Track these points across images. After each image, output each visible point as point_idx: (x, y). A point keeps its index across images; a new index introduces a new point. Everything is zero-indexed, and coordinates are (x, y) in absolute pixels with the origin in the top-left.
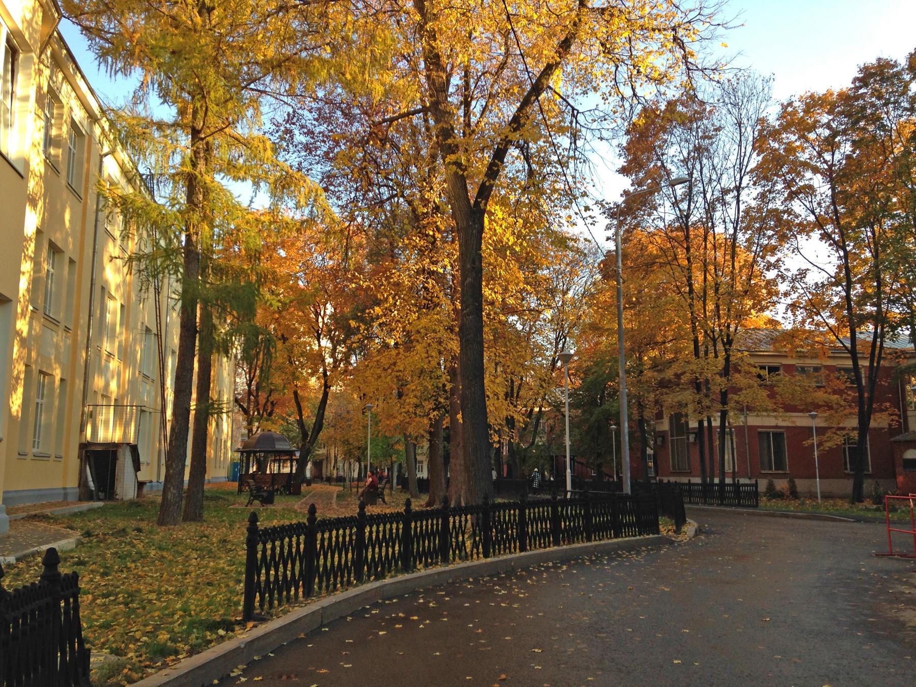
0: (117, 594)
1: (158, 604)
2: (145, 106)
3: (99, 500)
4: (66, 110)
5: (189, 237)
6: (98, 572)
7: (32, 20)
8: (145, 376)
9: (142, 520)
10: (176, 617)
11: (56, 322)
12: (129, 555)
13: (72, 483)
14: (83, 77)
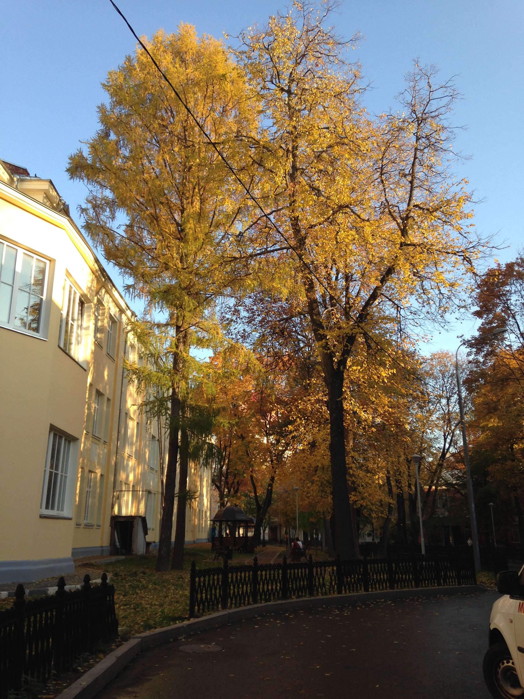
0: (130, 605)
1: (150, 610)
2: (151, 315)
3: (123, 555)
4: (106, 311)
5: (174, 389)
6: (121, 594)
7: (91, 286)
8: (152, 469)
9: (147, 568)
10: (158, 615)
11: (98, 439)
12: (138, 586)
13: (106, 543)
14: (116, 289)
